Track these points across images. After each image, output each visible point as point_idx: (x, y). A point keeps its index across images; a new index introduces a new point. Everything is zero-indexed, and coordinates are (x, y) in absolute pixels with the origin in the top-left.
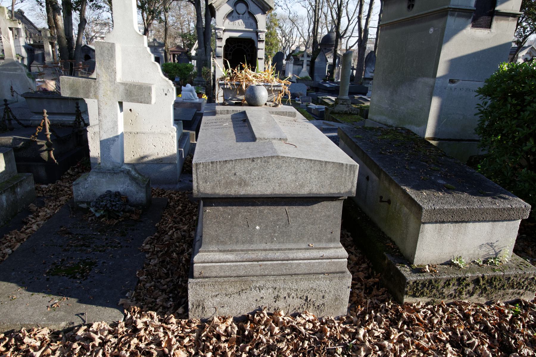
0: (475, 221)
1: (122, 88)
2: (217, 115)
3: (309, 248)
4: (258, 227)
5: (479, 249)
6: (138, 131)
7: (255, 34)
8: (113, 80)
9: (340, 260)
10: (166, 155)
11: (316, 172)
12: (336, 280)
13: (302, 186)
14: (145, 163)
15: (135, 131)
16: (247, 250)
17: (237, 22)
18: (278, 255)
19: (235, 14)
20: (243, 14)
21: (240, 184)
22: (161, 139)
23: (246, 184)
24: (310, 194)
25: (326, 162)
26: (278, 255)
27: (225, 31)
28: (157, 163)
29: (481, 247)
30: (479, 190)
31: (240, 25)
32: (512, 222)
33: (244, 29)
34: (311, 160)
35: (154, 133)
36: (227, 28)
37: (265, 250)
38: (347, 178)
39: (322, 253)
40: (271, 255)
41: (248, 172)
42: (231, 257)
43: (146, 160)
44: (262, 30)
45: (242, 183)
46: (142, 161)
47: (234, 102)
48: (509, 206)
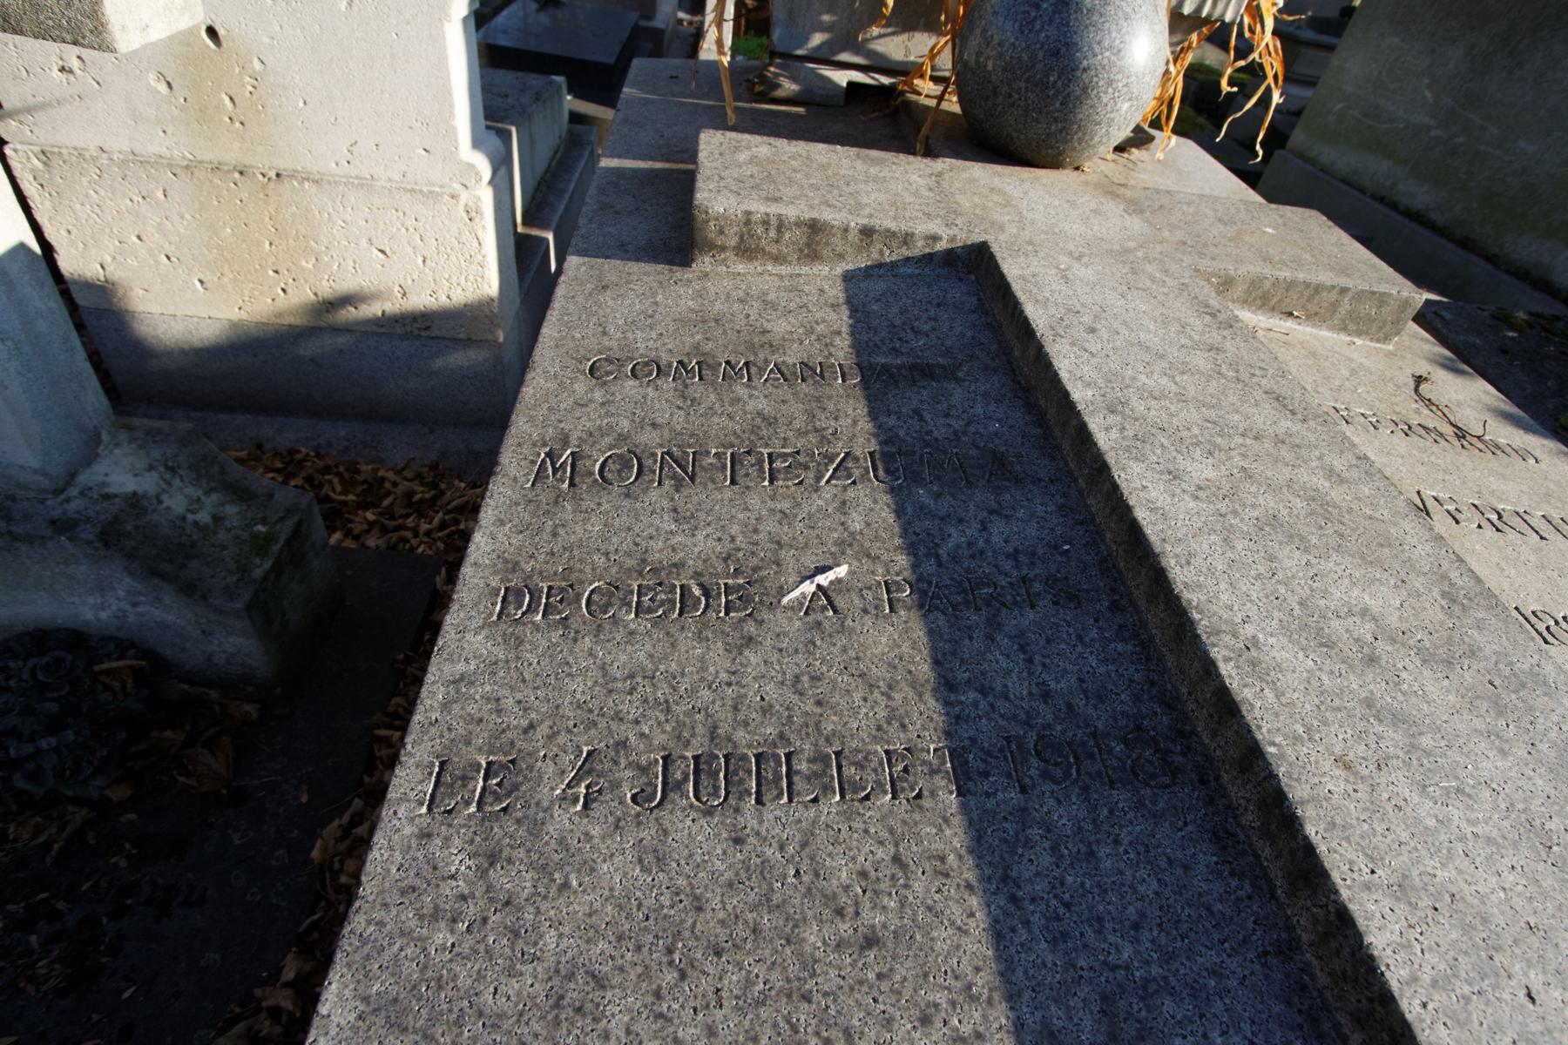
2: (704, 263)
6: (283, 164)
10: (443, 299)
14: (347, 329)
15: (262, 161)
16: (695, 368)
22: (410, 222)
28: (405, 336)
35: (365, 184)
43: (350, 314)
46: (330, 319)
47: (842, 78)
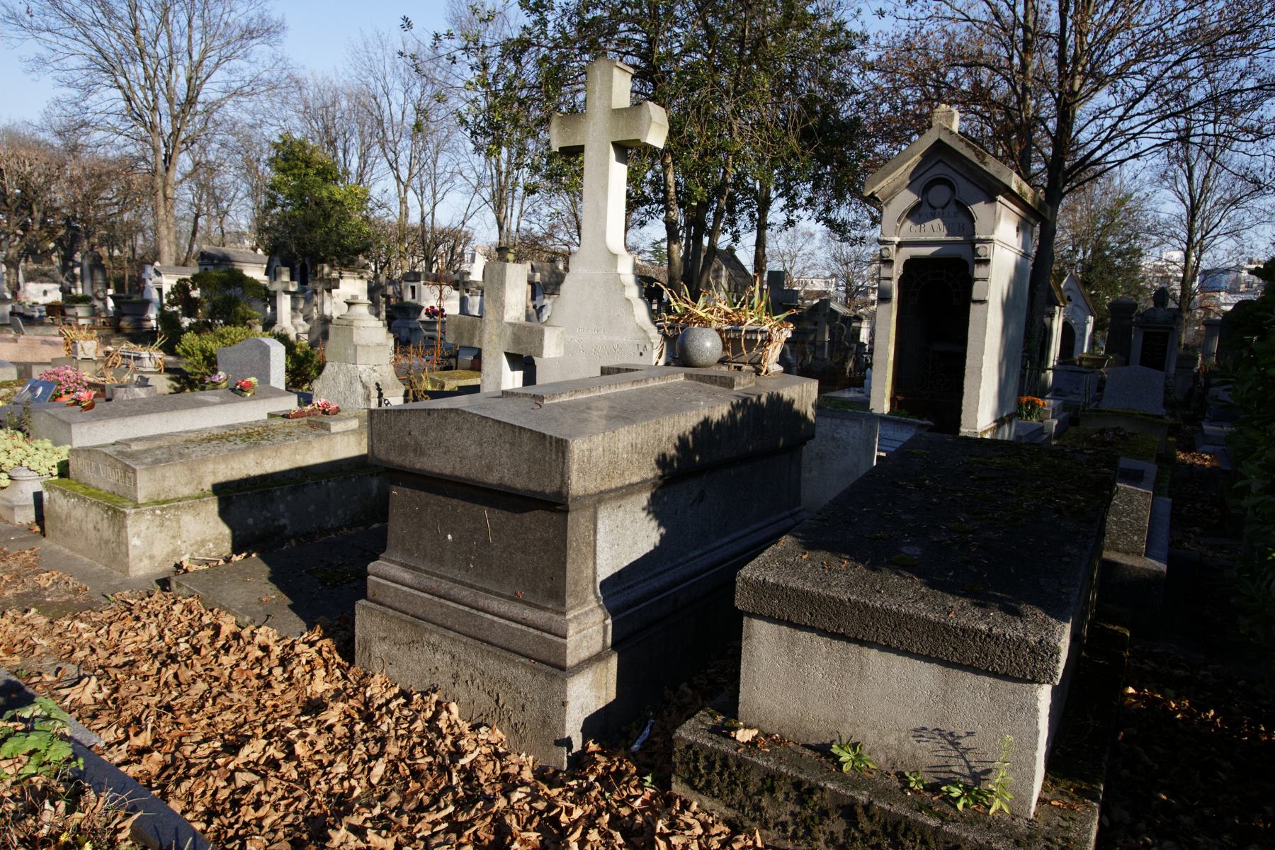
0: (887, 648)
1: (509, 331)
3: (513, 599)
4: (450, 537)
5: (913, 741)
7: (969, 247)
8: (500, 319)
9: (555, 639)
11: (507, 446)
12: (541, 678)
13: (490, 468)
17: (928, 224)
18: (465, 594)
19: (925, 209)
20: (943, 208)
21: (415, 451)
23: (423, 454)
24: (500, 485)
25: (520, 428)
26: (465, 594)
27: (900, 245)
29: (919, 732)
30: (943, 575)
31: (935, 230)
32: (1011, 685)
33: (943, 238)
34: (499, 422)
36: (904, 239)
37: (455, 581)
38: (554, 464)
39: (529, 614)
40: (458, 591)
41: (425, 432)
42: (407, 576)
44: (983, 237)
45: (418, 450)
48: (983, 627)
